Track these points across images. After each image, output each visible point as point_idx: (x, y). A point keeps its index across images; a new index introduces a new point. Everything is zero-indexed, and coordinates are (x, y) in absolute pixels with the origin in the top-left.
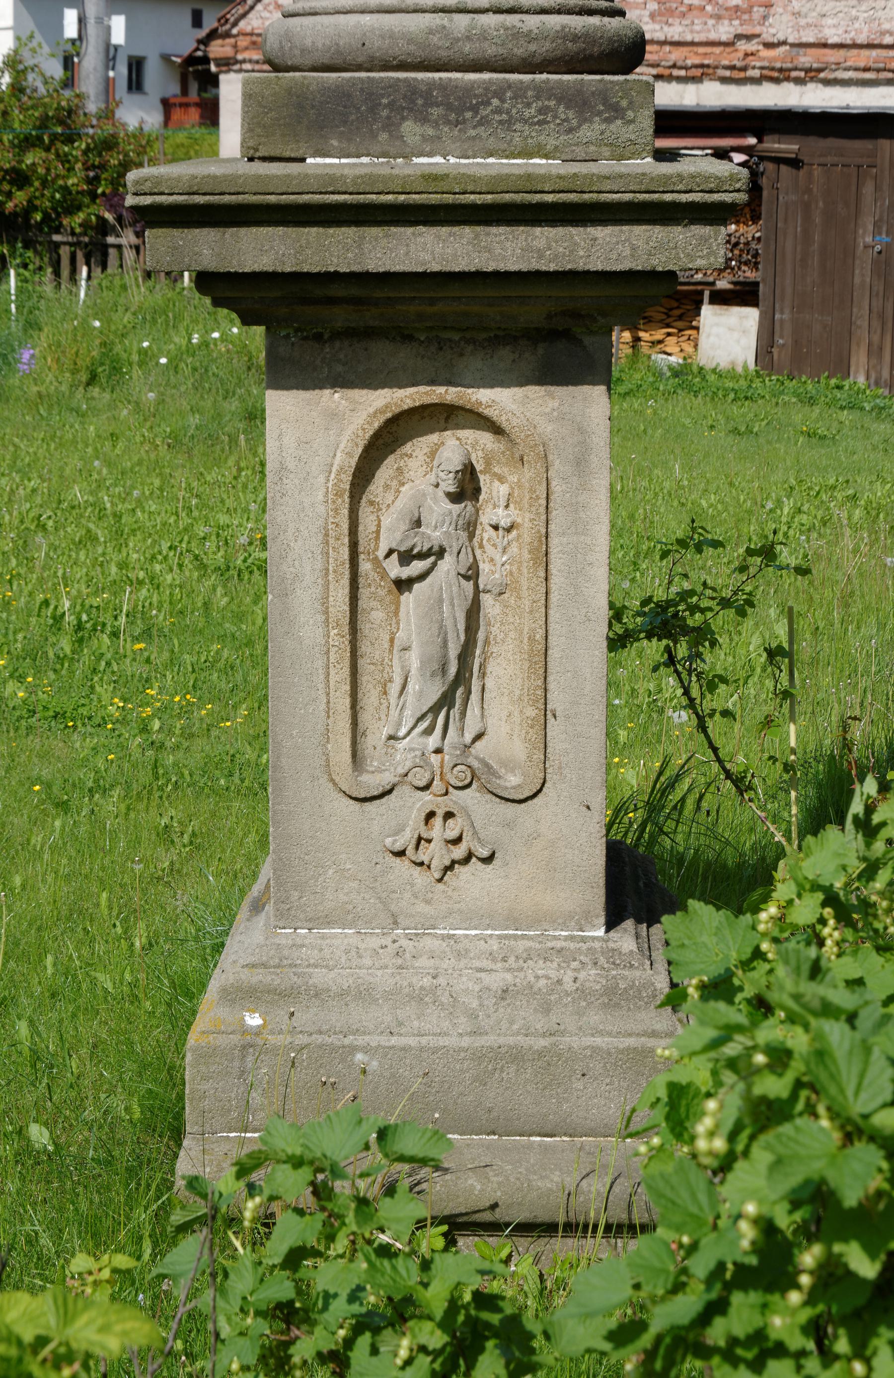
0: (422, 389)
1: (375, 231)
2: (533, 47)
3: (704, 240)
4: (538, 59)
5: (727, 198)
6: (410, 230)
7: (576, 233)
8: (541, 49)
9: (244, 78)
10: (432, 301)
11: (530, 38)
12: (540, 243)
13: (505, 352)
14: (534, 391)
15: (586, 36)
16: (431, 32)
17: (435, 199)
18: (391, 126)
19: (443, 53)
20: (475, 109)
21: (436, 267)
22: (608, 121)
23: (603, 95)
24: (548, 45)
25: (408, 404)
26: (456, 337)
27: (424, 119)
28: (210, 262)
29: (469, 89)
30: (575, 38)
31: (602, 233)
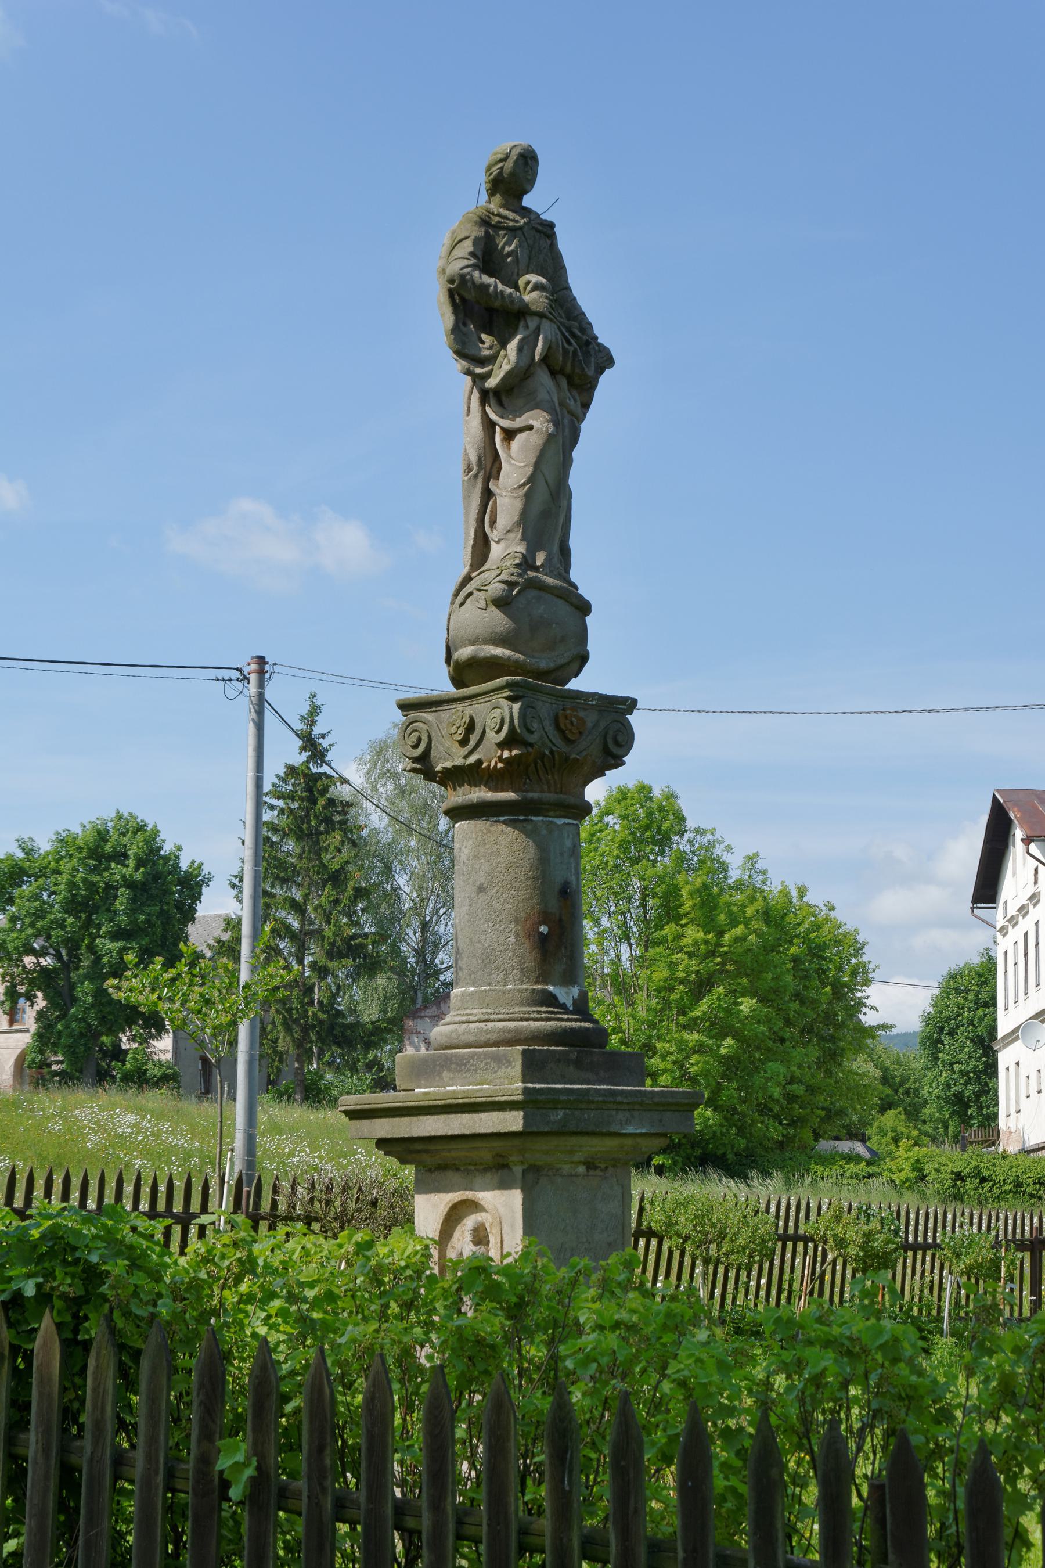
0: (462, 1192)
1: (415, 1118)
2: (488, 1036)
3: (515, 1117)
4: (491, 1042)
5: (515, 1098)
6: (425, 1117)
7: (476, 1116)
8: (493, 1037)
9: (524, 1052)
10: (449, 1150)
11: (487, 1032)
12: (465, 1121)
13: (488, 1175)
14: (497, 1192)
15: (517, 1031)
16: (452, 1032)
17: (426, 1103)
18: (440, 1074)
19: (456, 1041)
20: (465, 1065)
21: (433, 1134)
22: (507, 1067)
23: (505, 1056)
24: (495, 1035)
25: (457, 1200)
26: (473, 1168)
27: (450, 1070)
28: (383, 1134)
29: (463, 1056)
30: (509, 1031)
31: (484, 1116)
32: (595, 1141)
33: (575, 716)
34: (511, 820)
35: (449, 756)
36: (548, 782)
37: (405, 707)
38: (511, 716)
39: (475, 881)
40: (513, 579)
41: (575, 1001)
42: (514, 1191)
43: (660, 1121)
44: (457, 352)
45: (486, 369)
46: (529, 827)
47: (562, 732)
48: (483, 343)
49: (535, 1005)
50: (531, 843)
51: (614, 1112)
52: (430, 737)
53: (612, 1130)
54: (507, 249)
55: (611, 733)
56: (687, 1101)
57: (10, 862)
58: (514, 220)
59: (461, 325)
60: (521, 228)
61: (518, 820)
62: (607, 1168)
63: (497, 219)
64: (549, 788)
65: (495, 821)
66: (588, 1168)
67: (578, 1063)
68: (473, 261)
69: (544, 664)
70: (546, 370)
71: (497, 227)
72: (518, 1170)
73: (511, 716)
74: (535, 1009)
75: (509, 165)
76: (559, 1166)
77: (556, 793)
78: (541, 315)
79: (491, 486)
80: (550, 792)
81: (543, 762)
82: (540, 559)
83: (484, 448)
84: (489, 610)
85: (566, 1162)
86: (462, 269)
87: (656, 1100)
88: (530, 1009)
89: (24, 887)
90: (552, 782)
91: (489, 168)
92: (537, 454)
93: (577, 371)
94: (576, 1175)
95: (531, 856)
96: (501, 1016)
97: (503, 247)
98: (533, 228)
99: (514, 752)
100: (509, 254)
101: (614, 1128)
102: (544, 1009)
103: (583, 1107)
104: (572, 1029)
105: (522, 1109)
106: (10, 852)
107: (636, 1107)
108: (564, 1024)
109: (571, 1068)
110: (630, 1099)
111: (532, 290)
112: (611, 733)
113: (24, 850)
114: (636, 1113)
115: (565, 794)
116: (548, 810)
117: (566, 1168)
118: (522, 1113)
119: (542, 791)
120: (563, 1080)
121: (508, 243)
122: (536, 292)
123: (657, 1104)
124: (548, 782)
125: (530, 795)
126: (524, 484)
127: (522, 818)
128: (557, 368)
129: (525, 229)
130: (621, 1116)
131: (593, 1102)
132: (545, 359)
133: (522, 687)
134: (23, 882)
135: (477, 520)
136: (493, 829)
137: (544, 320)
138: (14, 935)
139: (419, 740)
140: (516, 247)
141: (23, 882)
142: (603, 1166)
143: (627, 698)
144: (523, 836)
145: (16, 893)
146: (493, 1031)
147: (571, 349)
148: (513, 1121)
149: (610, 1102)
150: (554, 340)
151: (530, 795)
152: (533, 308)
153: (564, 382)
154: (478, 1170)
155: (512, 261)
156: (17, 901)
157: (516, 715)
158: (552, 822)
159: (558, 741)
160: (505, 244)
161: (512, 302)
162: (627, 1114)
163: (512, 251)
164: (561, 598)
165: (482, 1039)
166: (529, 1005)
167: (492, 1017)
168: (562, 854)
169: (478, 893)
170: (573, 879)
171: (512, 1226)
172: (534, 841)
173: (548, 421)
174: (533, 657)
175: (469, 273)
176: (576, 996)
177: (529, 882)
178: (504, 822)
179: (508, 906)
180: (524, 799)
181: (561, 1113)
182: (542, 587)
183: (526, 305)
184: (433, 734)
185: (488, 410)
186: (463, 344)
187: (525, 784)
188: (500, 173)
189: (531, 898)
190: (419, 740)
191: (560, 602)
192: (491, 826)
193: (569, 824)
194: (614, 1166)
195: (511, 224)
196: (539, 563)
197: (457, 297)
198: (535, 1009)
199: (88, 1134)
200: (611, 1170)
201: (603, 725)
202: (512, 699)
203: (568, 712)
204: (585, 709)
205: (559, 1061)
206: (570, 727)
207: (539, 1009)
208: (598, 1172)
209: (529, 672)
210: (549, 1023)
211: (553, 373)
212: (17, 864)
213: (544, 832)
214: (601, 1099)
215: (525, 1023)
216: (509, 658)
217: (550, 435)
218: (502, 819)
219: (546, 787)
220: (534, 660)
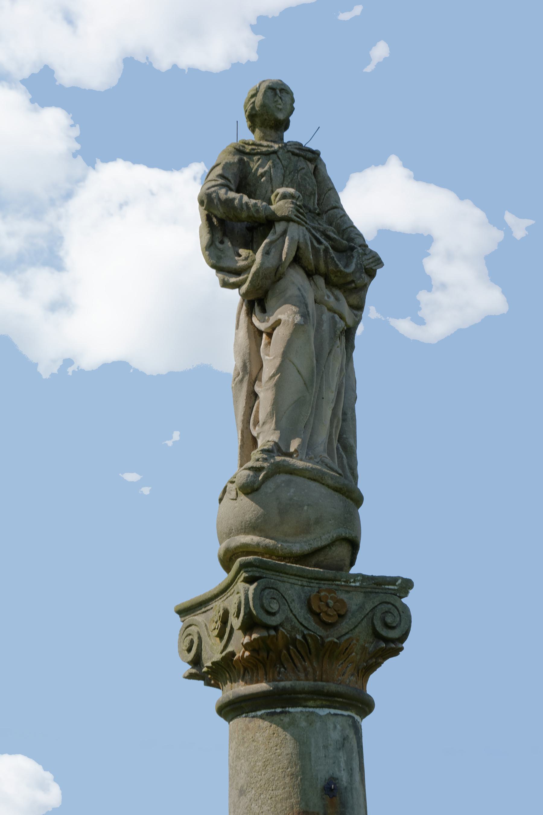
33: (332, 598)
34: (268, 714)
35: (213, 653)
36: (305, 669)
37: (184, 611)
38: (247, 599)
39: (237, 783)
40: (258, 464)
44: (213, 266)
45: (241, 278)
46: (286, 719)
47: (316, 615)
48: (240, 256)
50: (289, 737)
52: (200, 638)
54: (261, 171)
55: (378, 614)
58: (268, 146)
59: (217, 243)
60: (275, 152)
61: (275, 713)
63: (250, 147)
64: (306, 675)
65: (253, 717)
68: (220, 181)
69: (297, 548)
70: (301, 272)
71: (251, 154)
73: (247, 599)
75: (259, 99)
77: (315, 680)
78: (287, 219)
79: (257, 389)
80: (307, 679)
81: (296, 647)
82: (294, 445)
83: (250, 354)
84: (239, 499)
86: (208, 189)
90: (310, 670)
91: (245, 106)
92: (284, 344)
93: (331, 268)
95: (289, 750)
97: (257, 170)
98: (288, 151)
99: (254, 636)
100: (262, 175)
111: (280, 200)
112: (378, 614)
115: (327, 681)
116: (306, 700)
119: (299, 679)
121: (262, 166)
122: (282, 201)
124: (305, 669)
125: (282, 684)
126: (274, 375)
127: (279, 710)
128: (312, 267)
129: (279, 153)
132: (297, 260)
133: (258, 567)
135: (243, 421)
136: (251, 725)
137: (291, 224)
139: (192, 642)
140: (270, 168)
143: (393, 580)
144: (280, 730)
147: (322, 247)
150: (301, 240)
151: (282, 684)
152: (279, 214)
153: (321, 282)
155: (267, 181)
157: (251, 596)
158: (312, 713)
159: (312, 624)
160: (259, 166)
161: (257, 211)
163: (265, 172)
164: (315, 480)
168: (326, 747)
169: (239, 797)
170: (344, 777)
172: (292, 735)
173: (296, 313)
174: (286, 541)
175: (215, 191)
177: (287, 780)
178: (261, 717)
179: (266, 808)
180: (276, 688)
182: (293, 471)
183: (273, 213)
184: (202, 636)
185: (255, 320)
186: (219, 258)
187: (279, 673)
188: (253, 108)
189: (290, 797)
190: (192, 642)
191: (313, 484)
192: (250, 722)
193: (336, 715)
195: (264, 149)
196: (292, 450)
197: (215, 220)
201: (368, 607)
202: (249, 581)
203: (322, 594)
204: (348, 592)
206: (325, 609)
209: (290, 558)
211: (310, 275)
213: (304, 724)
216: (258, 544)
217: (296, 324)
218: (259, 713)
219: (302, 675)
220: (285, 545)
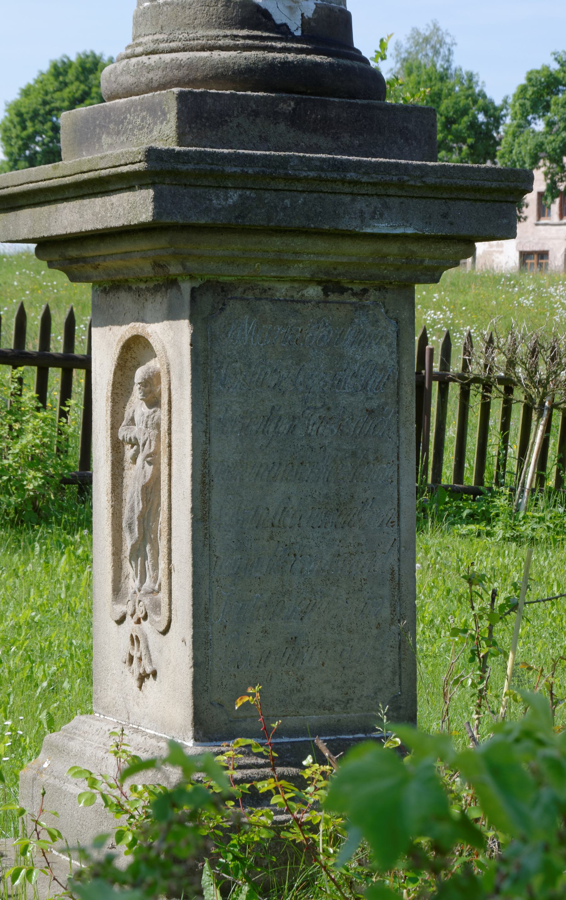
2: (150, 75)
4: (155, 84)
8: (156, 76)
9: (181, 97)
11: (150, 69)
14: (166, 324)
15: (190, 65)
24: (160, 73)
25: (128, 336)
30: (180, 66)
32: (321, 245)
41: (305, 22)
42: (182, 321)
43: (445, 216)
49: (231, 27)
51: (348, 199)
53: (343, 226)
56: (494, 185)
57: (545, 73)
62: (365, 291)
66: (326, 291)
67: (295, 120)
72: (186, 287)
74: (229, 32)
76: (266, 285)
85: (280, 279)
87: (430, 180)
88: (221, 33)
89: (560, 95)
94: (304, 301)
96: (173, 45)
101: (353, 225)
102: (245, 32)
103: (281, 185)
104: (285, 63)
105: (152, 185)
106: (546, 63)
107: (391, 191)
108: (271, 55)
109: (282, 127)
110: (376, 178)
113: (559, 62)
114: (394, 202)
117: (282, 290)
118: (151, 192)
120: (263, 141)
123: (435, 188)
130: (360, 204)
131: (299, 180)
134: (559, 91)
138: (551, 138)
141: (559, 91)
142: (357, 287)
145: (554, 99)
146: (166, 66)
148: (135, 207)
149: (334, 181)
154: (148, 289)
156: (553, 107)
162: (376, 202)
165: (143, 79)
166: (220, 26)
167: (162, 46)
171: (180, 378)
176: (309, 13)
181: (234, 197)
194: (379, 288)
198: (229, 32)
199: (558, 308)
200: (373, 296)
205: (256, 114)
207: (235, 32)
208: (347, 297)
210: (246, 54)
212: (551, 75)
214: (312, 174)
215: (206, 54)
